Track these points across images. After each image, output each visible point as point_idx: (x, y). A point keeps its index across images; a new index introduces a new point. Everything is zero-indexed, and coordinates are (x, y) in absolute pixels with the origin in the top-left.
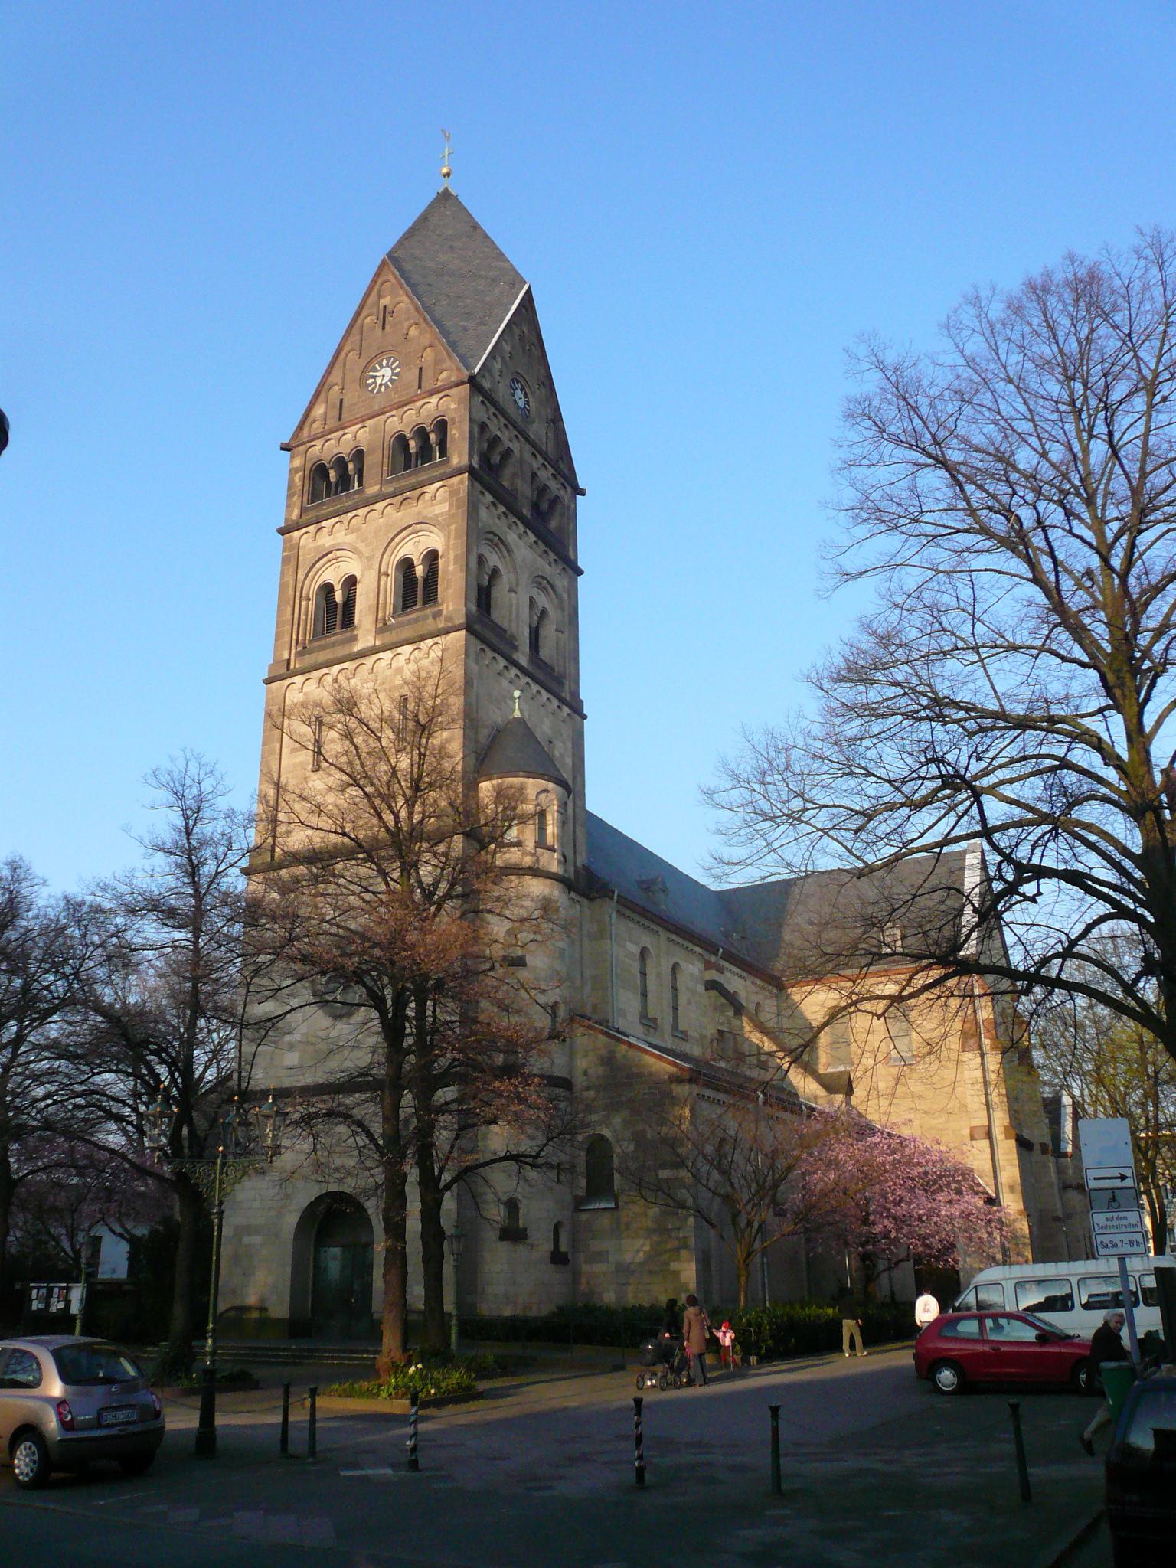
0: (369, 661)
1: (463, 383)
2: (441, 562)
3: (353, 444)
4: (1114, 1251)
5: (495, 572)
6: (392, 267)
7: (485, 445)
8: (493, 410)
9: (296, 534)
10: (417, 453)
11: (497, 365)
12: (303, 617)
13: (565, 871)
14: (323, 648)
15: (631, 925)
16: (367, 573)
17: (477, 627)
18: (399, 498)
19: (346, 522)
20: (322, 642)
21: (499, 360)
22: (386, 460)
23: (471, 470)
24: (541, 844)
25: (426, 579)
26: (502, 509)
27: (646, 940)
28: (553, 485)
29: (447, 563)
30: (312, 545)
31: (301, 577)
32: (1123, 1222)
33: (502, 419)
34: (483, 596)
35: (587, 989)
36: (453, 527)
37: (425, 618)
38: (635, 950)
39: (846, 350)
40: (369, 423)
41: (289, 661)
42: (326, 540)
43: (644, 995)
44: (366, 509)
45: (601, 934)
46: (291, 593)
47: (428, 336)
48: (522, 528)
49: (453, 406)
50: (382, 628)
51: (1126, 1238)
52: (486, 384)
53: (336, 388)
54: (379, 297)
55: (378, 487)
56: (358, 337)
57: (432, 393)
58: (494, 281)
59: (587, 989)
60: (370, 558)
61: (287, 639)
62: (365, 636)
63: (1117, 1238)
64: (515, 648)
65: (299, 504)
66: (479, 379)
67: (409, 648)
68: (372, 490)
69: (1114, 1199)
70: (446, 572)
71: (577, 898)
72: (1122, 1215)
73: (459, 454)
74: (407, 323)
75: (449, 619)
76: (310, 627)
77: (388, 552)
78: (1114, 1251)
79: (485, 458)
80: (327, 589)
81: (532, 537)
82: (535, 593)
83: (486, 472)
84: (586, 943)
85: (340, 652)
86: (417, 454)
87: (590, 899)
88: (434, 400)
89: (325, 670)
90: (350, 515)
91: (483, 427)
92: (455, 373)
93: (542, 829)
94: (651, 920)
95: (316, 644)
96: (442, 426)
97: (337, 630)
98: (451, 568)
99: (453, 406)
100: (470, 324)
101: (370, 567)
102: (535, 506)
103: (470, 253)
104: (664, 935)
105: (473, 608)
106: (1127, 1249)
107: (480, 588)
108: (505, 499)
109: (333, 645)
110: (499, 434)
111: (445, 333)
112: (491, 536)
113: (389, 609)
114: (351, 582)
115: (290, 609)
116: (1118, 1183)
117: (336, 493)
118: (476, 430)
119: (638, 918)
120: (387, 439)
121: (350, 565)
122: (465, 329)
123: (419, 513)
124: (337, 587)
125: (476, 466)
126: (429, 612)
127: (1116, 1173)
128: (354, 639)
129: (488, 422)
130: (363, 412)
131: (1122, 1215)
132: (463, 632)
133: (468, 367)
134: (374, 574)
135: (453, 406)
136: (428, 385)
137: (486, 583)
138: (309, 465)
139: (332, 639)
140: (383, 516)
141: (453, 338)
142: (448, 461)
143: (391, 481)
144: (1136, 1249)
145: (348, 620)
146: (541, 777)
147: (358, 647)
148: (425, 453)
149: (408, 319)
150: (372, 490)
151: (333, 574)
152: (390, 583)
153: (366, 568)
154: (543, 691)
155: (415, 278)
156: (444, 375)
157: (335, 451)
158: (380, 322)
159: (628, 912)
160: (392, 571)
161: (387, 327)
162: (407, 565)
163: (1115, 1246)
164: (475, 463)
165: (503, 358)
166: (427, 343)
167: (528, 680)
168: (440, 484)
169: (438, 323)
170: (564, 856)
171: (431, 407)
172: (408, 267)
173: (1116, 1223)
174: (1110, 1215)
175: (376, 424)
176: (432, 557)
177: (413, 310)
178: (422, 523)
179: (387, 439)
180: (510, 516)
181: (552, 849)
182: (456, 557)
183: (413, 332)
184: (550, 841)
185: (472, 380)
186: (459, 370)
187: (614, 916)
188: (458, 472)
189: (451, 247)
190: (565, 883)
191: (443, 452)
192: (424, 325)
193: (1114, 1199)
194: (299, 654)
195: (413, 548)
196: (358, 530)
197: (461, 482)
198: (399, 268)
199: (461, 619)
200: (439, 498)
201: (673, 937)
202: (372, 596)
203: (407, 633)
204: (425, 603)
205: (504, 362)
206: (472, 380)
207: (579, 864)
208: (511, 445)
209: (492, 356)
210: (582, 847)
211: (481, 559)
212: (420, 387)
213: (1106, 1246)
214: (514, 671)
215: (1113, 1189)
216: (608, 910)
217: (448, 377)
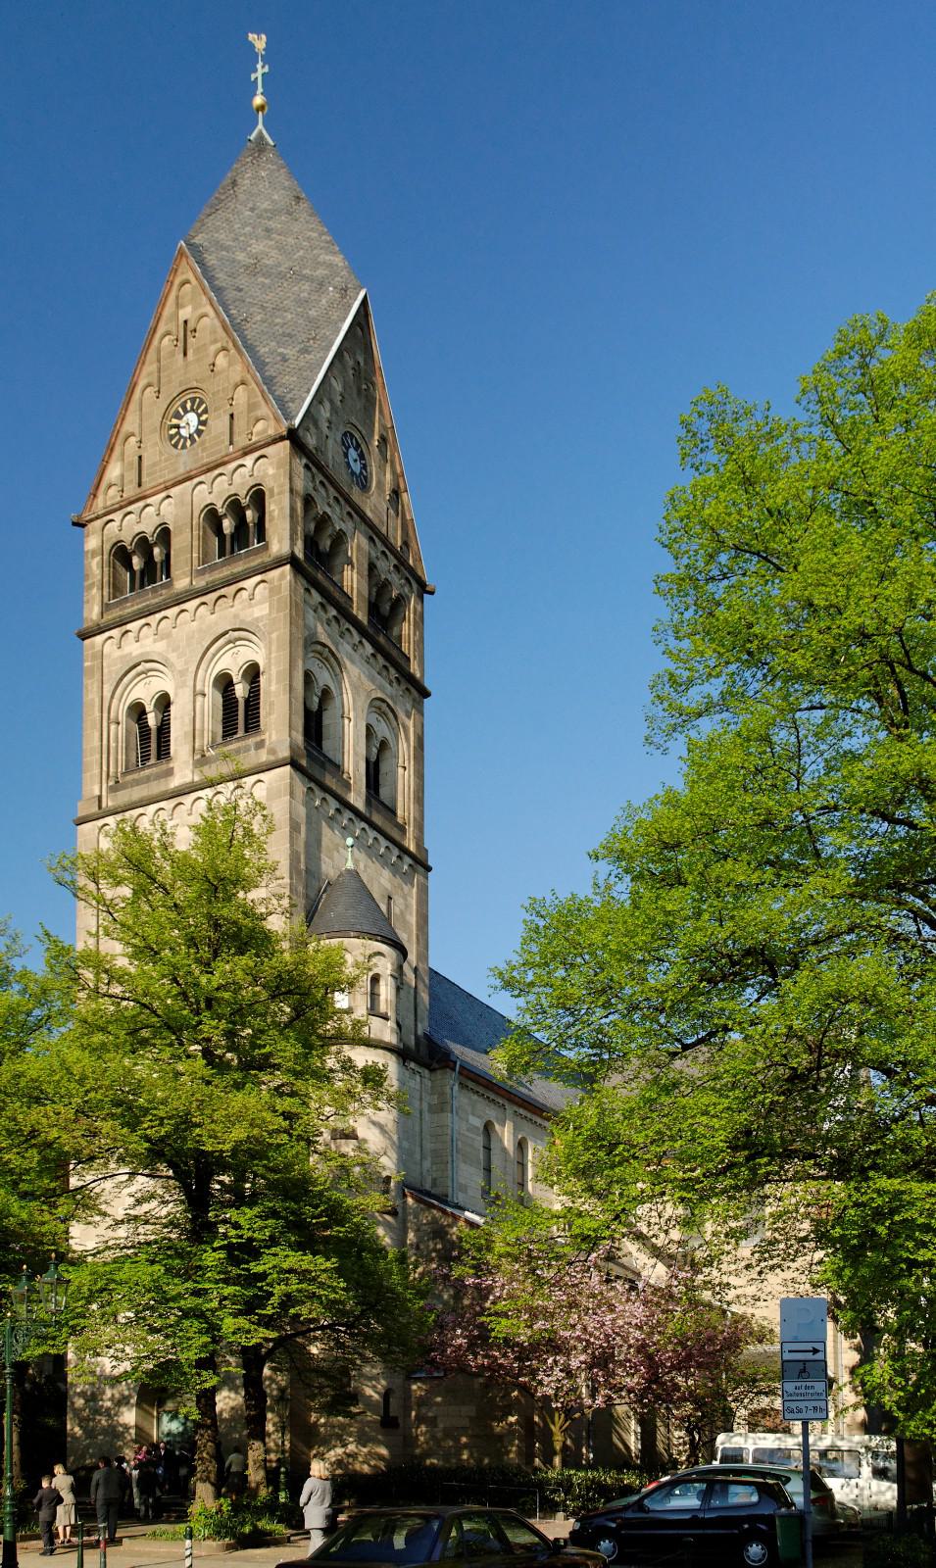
0: (188, 799)
1: (282, 438)
2: (262, 679)
3: (157, 521)
4: (800, 1416)
5: (326, 694)
6: (192, 260)
7: (312, 526)
8: (321, 478)
9: (99, 639)
10: (235, 530)
11: (325, 412)
12: (113, 745)
13: (400, 1040)
14: (137, 782)
15: (475, 1097)
16: (180, 691)
17: (304, 762)
18: (214, 595)
19: (154, 625)
20: (135, 776)
21: (327, 405)
22: (195, 543)
23: (292, 560)
24: (373, 1011)
25: (247, 701)
26: (333, 612)
27: (491, 1113)
28: (396, 579)
29: (269, 681)
30: (118, 653)
31: (107, 694)
32: (811, 1391)
33: (331, 490)
34: (314, 724)
35: (427, 1164)
36: (274, 636)
37: (247, 749)
38: (479, 1123)
39: (685, 425)
40: (173, 491)
41: (100, 798)
42: (133, 649)
43: (488, 1170)
44: (176, 609)
45: (442, 1106)
46: (97, 714)
47: (239, 367)
48: (357, 637)
49: (273, 471)
50: (202, 761)
51: (811, 1405)
52: (311, 441)
53: (133, 440)
54: (178, 306)
55: (188, 580)
56: (155, 366)
57: (246, 452)
58: (321, 285)
59: (427, 1164)
60: (182, 673)
61: (97, 771)
62: (182, 768)
63: (802, 1405)
64: (347, 786)
65: (98, 599)
66: (301, 433)
67: (231, 785)
68: (181, 583)
69: (804, 1370)
70: (268, 693)
71: (417, 1068)
72: (808, 1384)
73: (280, 539)
74: (213, 348)
75: (272, 751)
76: (122, 757)
77: (203, 666)
78: (800, 1416)
79: (311, 543)
80: (138, 711)
81: (369, 649)
82: (374, 718)
83: (315, 564)
84: (427, 1116)
85: (156, 788)
86: (232, 536)
87: (432, 1070)
88: (249, 461)
89: (140, 810)
90: (158, 616)
91: (308, 501)
92: (272, 422)
93: (374, 996)
94: (497, 1093)
95: (129, 778)
96: (258, 497)
97: (153, 761)
98: (273, 688)
99: (271, 471)
100: (290, 352)
101: (183, 685)
102: (373, 608)
103: (291, 241)
104: (510, 1108)
105: (299, 738)
106: (810, 1414)
107: (307, 712)
108: (334, 600)
109: (148, 779)
110: (328, 510)
111: (260, 365)
112: (319, 647)
113: (207, 739)
114: (164, 703)
115: (97, 734)
116: (810, 1356)
117: (142, 586)
118: (299, 505)
119: (481, 1090)
120: (196, 514)
121: (163, 683)
122: (285, 359)
123: (236, 616)
124: (149, 708)
125: (300, 555)
126: (252, 741)
127: (809, 1346)
128: (170, 773)
129: (313, 493)
130: (169, 476)
131: (808, 1384)
132: (288, 767)
133: (289, 417)
134: (188, 693)
135: (271, 471)
136: (241, 441)
137: (315, 707)
138: (107, 547)
139: (147, 772)
140: (195, 621)
141: (271, 372)
142: (266, 548)
143: (202, 573)
144: (818, 1415)
145: (164, 752)
146: (373, 937)
147: (175, 782)
148: (241, 537)
149: (215, 341)
150: (181, 583)
151: (144, 692)
152: (212, 701)
153: (179, 686)
154: (381, 839)
155: (222, 278)
156: (260, 425)
157: (138, 529)
158: (181, 344)
159: (471, 1085)
160: (209, 689)
161: (190, 352)
162: (138, 711)
163: (800, 1411)
164: (300, 554)
165: (331, 401)
166: (238, 379)
167: (363, 825)
168: (258, 578)
169: (251, 349)
170: (398, 1024)
171: (237, 481)
172: (211, 259)
173: (803, 1391)
174: (799, 1384)
175: (182, 494)
176: (253, 673)
177: (220, 330)
178: (239, 632)
179: (196, 514)
180: (343, 621)
181: (386, 1018)
182: (278, 673)
183: (221, 361)
184: (383, 1008)
185: (292, 436)
186: (277, 419)
187: (456, 1088)
188: (278, 563)
189: (267, 230)
190: (402, 1053)
191: (261, 535)
192: (233, 351)
193: (804, 1370)
194: (112, 790)
195: (232, 661)
196: (168, 636)
197: (282, 576)
198: (201, 263)
199: (284, 753)
200: (257, 596)
201: (521, 1111)
202: (188, 720)
203: (226, 769)
204: (247, 730)
205: (334, 410)
206: (292, 436)
207: (420, 1032)
208: (343, 527)
209: (318, 398)
210: (424, 1012)
211: (308, 678)
212: (231, 443)
213: (792, 1412)
214: (348, 814)
215: (805, 1362)
216: (450, 1081)
217: (265, 430)
